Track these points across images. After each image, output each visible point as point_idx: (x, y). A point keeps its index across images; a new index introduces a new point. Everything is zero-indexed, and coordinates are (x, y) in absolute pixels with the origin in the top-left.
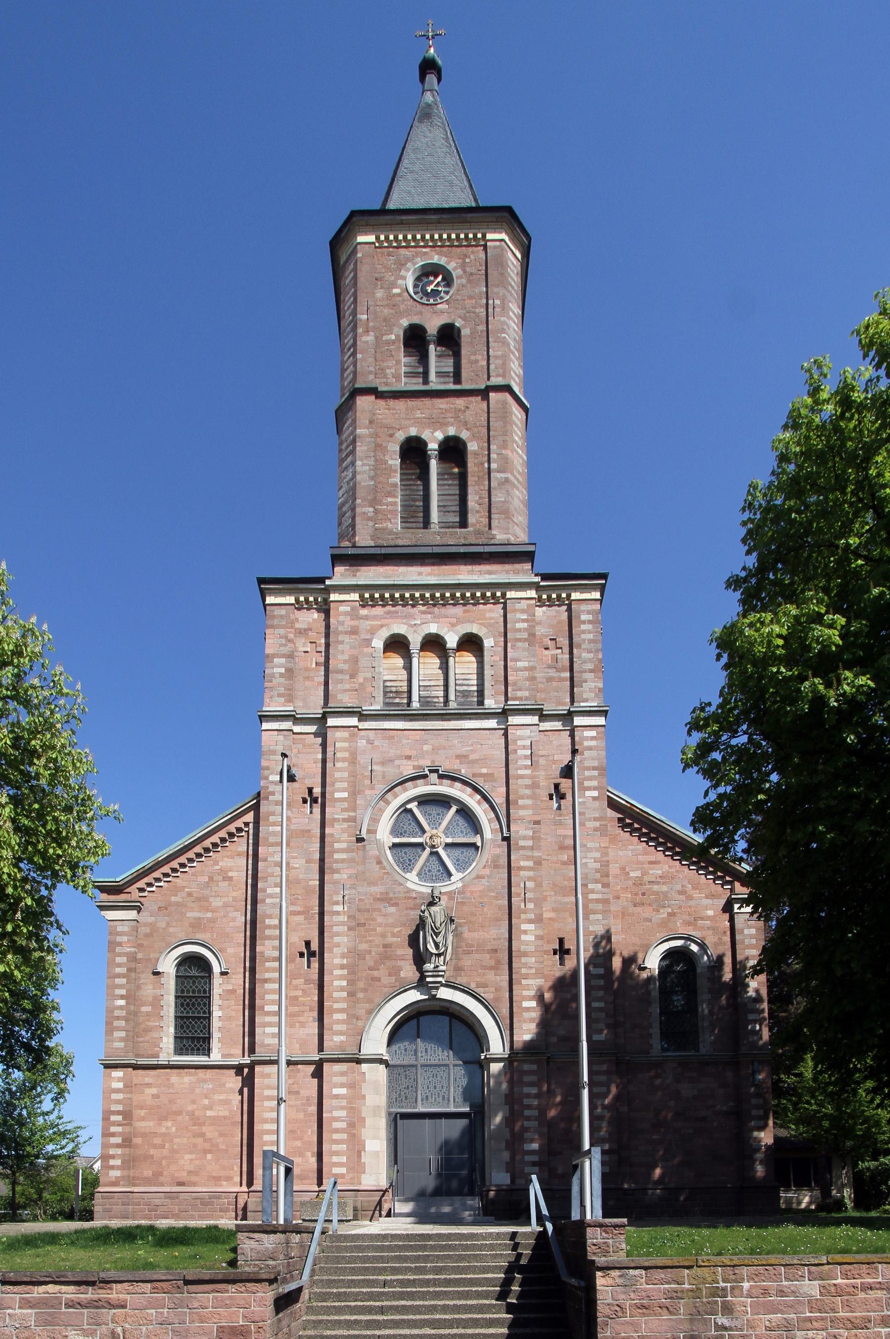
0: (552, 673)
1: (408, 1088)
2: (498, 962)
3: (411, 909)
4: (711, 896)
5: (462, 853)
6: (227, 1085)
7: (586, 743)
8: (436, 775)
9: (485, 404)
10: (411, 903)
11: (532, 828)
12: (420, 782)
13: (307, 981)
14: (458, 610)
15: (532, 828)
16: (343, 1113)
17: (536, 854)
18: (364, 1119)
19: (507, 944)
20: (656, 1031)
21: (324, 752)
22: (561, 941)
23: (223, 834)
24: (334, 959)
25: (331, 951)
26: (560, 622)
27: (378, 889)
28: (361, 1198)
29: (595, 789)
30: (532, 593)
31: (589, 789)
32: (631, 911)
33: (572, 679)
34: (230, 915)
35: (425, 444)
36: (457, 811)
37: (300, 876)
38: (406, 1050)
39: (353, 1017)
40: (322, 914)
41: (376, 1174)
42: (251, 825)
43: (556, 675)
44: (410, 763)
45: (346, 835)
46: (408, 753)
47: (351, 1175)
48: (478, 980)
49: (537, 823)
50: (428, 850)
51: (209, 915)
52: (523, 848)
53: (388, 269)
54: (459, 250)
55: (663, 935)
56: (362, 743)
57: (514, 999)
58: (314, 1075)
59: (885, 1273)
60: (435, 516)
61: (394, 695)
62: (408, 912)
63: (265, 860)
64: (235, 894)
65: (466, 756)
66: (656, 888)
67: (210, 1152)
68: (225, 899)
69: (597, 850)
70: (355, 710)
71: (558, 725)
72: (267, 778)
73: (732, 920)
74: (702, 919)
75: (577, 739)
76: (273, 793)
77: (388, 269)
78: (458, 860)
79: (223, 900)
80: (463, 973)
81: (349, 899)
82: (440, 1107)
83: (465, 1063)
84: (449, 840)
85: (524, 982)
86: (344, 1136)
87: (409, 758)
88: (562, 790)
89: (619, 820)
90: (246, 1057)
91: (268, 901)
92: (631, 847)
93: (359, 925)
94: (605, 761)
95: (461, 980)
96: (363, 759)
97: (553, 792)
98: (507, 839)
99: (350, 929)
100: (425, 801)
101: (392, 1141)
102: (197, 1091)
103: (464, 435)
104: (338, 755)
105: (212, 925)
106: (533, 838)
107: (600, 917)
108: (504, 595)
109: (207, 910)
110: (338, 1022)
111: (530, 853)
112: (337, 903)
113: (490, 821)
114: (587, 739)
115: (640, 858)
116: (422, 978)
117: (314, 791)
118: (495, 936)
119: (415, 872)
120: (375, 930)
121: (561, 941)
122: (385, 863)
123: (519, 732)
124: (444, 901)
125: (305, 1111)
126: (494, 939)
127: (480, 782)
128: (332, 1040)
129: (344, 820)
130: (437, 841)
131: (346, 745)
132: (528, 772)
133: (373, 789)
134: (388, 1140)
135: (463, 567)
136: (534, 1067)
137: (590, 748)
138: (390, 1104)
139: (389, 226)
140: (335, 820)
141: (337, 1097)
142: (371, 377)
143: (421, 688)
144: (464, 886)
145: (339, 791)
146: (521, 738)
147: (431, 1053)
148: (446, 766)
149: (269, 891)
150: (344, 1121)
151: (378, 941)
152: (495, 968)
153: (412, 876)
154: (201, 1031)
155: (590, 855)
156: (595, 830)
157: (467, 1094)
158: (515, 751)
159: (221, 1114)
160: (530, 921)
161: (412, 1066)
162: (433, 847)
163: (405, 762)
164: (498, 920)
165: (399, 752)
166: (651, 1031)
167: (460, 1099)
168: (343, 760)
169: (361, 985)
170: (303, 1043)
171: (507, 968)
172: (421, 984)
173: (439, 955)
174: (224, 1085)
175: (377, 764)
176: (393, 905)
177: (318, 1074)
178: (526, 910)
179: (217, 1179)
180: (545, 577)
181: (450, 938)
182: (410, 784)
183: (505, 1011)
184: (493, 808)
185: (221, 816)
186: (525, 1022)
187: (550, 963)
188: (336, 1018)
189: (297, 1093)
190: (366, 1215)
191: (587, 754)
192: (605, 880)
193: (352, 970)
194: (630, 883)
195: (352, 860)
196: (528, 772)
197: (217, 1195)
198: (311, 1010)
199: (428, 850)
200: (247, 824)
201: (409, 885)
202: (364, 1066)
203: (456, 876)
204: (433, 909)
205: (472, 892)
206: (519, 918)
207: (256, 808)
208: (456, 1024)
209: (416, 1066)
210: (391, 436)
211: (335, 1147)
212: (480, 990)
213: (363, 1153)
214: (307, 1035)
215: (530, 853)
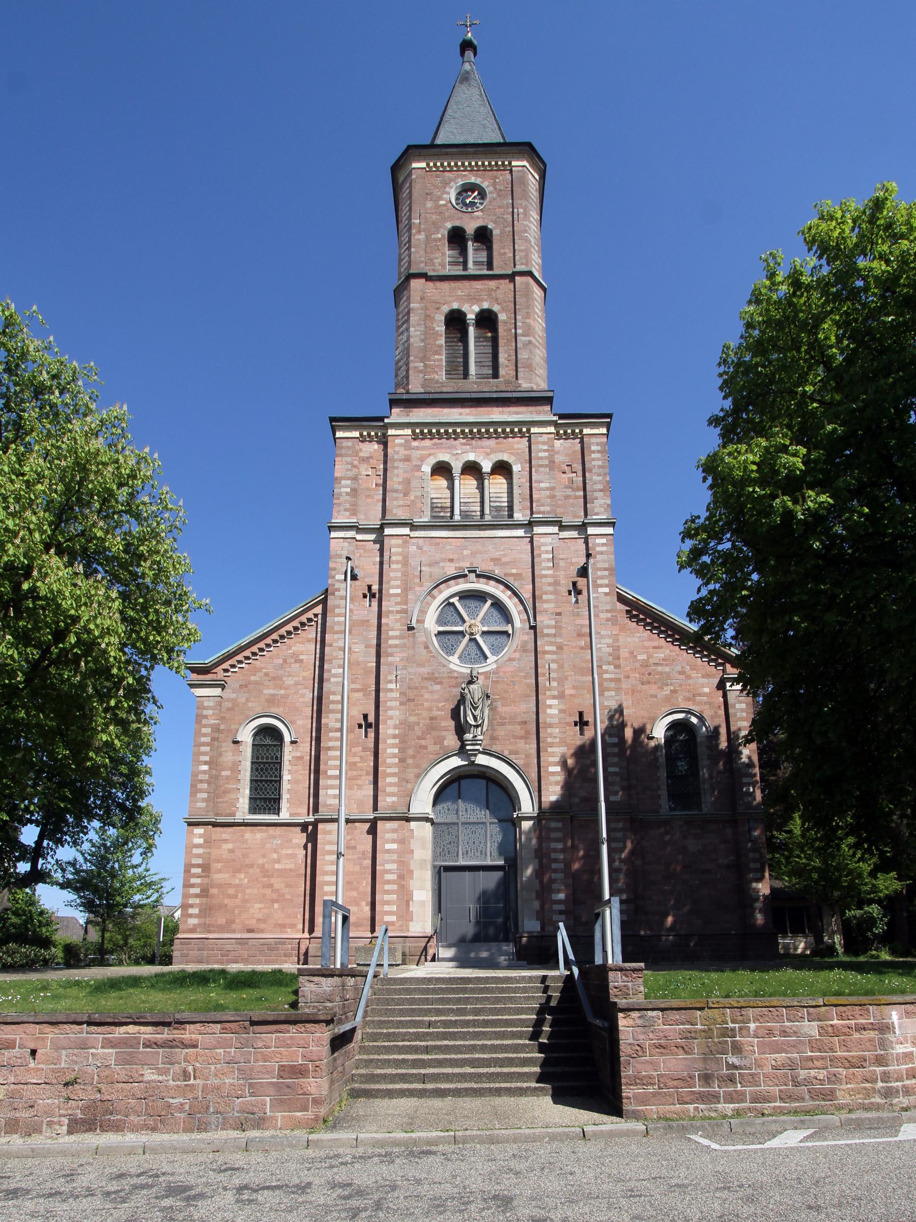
4: (707, 676)
6: (294, 841)
7: (598, 549)
9: (512, 285)
10: (454, 682)
13: (365, 749)
14: (492, 442)
16: (394, 866)
17: (559, 640)
18: (412, 872)
19: (535, 717)
20: (664, 792)
21: (382, 556)
22: (581, 714)
23: (296, 623)
24: (388, 729)
26: (574, 452)
27: (425, 670)
28: (409, 943)
29: (606, 586)
30: (552, 429)
31: (601, 586)
33: (585, 497)
34: (300, 692)
35: (465, 315)
36: (492, 604)
38: (449, 810)
39: (403, 780)
40: (378, 691)
41: (423, 922)
42: (320, 616)
45: (399, 624)
47: (400, 923)
49: (559, 614)
51: (282, 692)
52: (548, 635)
53: (436, 187)
56: (413, 549)
58: (369, 832)
62: (451, 689)
63: (331, 645)
64: (304, 674)
65: (499, 559)
66: (660, 669)
69: (609, 637)
71: (574, 534)
72: (334, 577)
73: (725, 696)
74: (700, 695)
75: (590, 545)
77: (436, 187)
78: (493, 645)
83: (500, 821)
84: (485, 629)
85: (550, 750)
86: (395, 887)
87: (451, 560)
89: (627, 612)
91: (332, 680)
92: (637, 635)
93: (409, 700)
95: (496, 748)
96: (414, 562)
98: (533, 628)
99: (401, 704)
100: (465, 596)
101: (437, 892)
102: (268, 846)
103: (496, 308)
104: (393, 558)
105: (284, 700)
106: (555, 627)
107: (613, 693)
108: (528, 431)
109: (281, 688)
110: (391, 785)
111: (553, 640)
112: (391, 682)
113: (519, 613)
114: (599, 545)
115: (646, 643)
116: (463, 746)
119: (456, 656)
121: (581, 714)
122: (431, 648)
123: (543, 540)
125: (361, 864)
126: (524, 713)
127: (511, 581)
129: (398, 612)
130: (475, 630)
131: (400, 550)
133: (422, 586)
134: (433, 890)
135: (495, 409)
136: (560, 825)
137: (601, 553)
138: (435, 857)
139: (437, 156)
140: (390, 612)
141: (389, 851)
142: (422, 265)
144: (498, 668)
145: (393, 587)
146: (544, 545)
147: (470, 812)
148: (482, 567)
149: (333, 671)
151: (425, 714)
152: (525, 737)
153: (454, 659)
155: (603, 641)
156: (608, 620)
158: (540, 555)
159: (288, 867)
160: (554, 697)
161: (454, 824)
162: (472, 634)
163: (448, 564)
164: (527, 696)
165: (443, 556)
166: (660, 792)
168: (398, 562)
169: (410, 752)
170: (360, 804)
171: (535, 736)
172: (462, 751)
174: (291, 841)
175: (425, 566)
176: (437, 684)
177: (373, 831)
178: (550, 687)
179: (283, 927)
180: (561, 417)
182: (452, 582)
183: (534, 775)
187: (572, 733)
188: (388, 782)
189: (354, 848)
191: (599, 557)
192: (617, 662)
193: (403, 739)
194: (638, 665)
195: (403, 646)
196: (550, 572)
200: (316, 615)
201: (452, 666)
203: (492, 659)
204: (472, 687)
205: (505, 672)
206: (545, 694)
207: (324, 602)
209: (457, 824)
213: (411, 902)
214: (364, 796)
215: (553, 640)
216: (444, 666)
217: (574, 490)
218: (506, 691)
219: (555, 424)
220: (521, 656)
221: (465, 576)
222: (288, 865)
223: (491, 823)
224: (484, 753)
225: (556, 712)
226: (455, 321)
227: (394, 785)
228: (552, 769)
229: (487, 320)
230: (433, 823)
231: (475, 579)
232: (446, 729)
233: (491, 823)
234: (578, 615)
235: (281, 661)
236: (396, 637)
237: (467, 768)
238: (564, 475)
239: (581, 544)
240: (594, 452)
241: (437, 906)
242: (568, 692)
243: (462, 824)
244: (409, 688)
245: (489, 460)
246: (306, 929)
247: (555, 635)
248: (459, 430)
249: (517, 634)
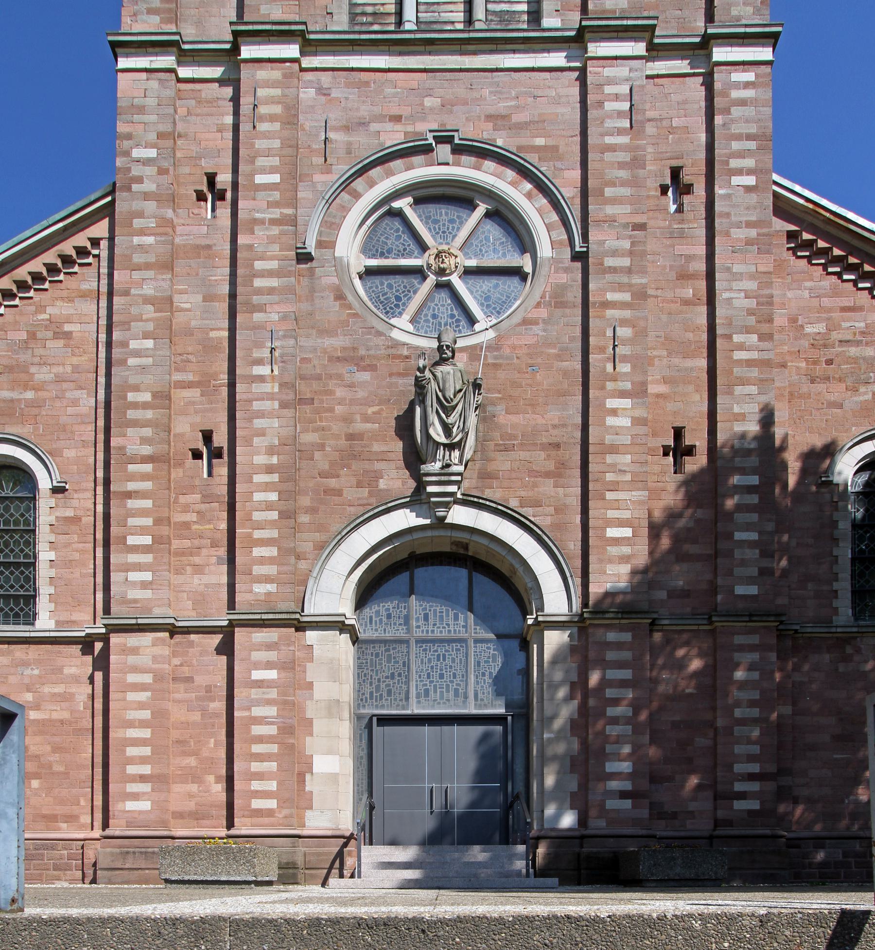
1: (392, 676)
2: (562, 465)
3: (400, 375)
5: (496, 286)
6: (66, 671)
7: (735, 94)
8: (447, 148)
10: (401, 366)
11: (630, 237)
12: (417, 159)
13: (207, 498)
15: (630, 237)
16: (271, 711)
17: (637, 280)
18: (310, 722)
19: (578, 434)
20: (844, 585)
21: (236, 113)
22: (678, 433)
23: (51, 257)
24: (254, 456)
25: (249, 443)
27: (337, 343)
28: (302, 847)
29: (750, 172)
31: (739, 172)
32: (805, 389)
34: (68, 395)
36: (488, 215)
37: (193, 323)
38: (389, 616)
39: (289, 553)
40: (232, 385)
41: (333, 807)
42: (104, 244)
44: (398, 127)
45: (276, 247)
46: (395, 111)
47: (285, 812)
48: (523, 494)
49: (642, 227)
50: (432, 279)
51: (30, 395)
52: (614, 270)
55: (858, 431)
56: (308, 94)
57: (592, 523)
58: (219, 651)
59: (822, 948)
61: (370, 19)
62: (394, 380)
63: (126, 293)
64: (75, 360)
65: (503, 117)
66: (853, 351)
67: (37, 776)
68: (60, 369)
69: (752, 277)
70: (293, 28)
71: (681, 66)
72: (127, 154)
75: (717, 86)
76: (139, 180)
78: (487, 298)
79: (55, 369)
80: (495, 483)
81: (282, 356)
82: (451, 707)
83: (499, 636)
84: (472, 263)
86: (274, 748)
87: (397, 119)
89: (791, 236)
90: (100, 622)
91: (131, 361)
92: (808, 284)
93: (302, 401)
94: (770, 125)
95: (493, 493)
96: (309, 122)
97: (668, 181)
98: (581, 257)
99: (284, 405)
100: (429, 195)
101: (365, 761)
102: (12, 679)
104: (263, 110)
105: (35, 411)
106: (631, 253)
107: (753, 389)
109: (26, 387)
111: (625, 279)
112: (259, 362)
113: (549, 228)
114: (737, 85)
115: (826, 302)
116: (421, 487)
117: (219, 179)
118: (556, 422)
119: (406, 317)
120: (331, 410)
121: (678, 433)
122: (350, 298)
123: (609, 71)
124: (461, 360)
125: (204, 711)
126: (555, 427)
128: (251, 591)
129: (273, 222)
130: (449, 263)
131: (277, 92)
133: (329, 172)
134: (357, 759)
136: (627, 637)
138: (360, 698)
140: (255, 221)
141: (260, 684)
143: (421, 8)
144: (499, 338)
145: (263, 171)
146: (611, 81)
147: (433, 617)
148: (469, 131)
149: (134, 345)
150: (272, 723)
151: (337, 427)
152: (557, 474)
153: (403, 321)
154: (22, 587)
155: (735, 285)
156: (749, 242)
157: (500, 685)
158: (600, 104)
159: (55, 716)
160: (623, 394)
161: (400, 641)
162: (441, 272)
163: (389, 126)
165: (377, 110)
166: (836, 586)
167: (487, 689)
168: (272, 118)
169: (305, 501)
170: (200, 600)
171: (577, 472)
172: (418, 499)
174: (60, 670)
175: (336, 129)
176: (364, 369)
177: (227, 648)
178: (614, 374)
179: (51, 819)
181: (472, 420)
182: (398, 163)
183: (574, 546)
184: (556, 205)
185: (45, 223)
186: (610, 561)
187: (657, 469)
188: (260, 553)
189: (190, 680)
190: (313, 877)
191: (736, 112)
192: (765, 328)
193: (289, 480)
194: (806, 344)
195: (289, 290)
196: (624, 140)
198: (214, 545)
199: (432, 279)
200: (95, 242)
201: (396, 334)
202: (311, 636)
204: (441, 370)
205: (514, 347)
206: (603, 388)
207: (109, 211)
208: (482, 582)
209: (407, 642)
211: (255, 767)
212: (528, 511)
213: (308, 777)
214: (206, 586)
215: (625, 279)
216: (379, 334)
218: (515, 384)
220: (551, 316)
221: (427, 150)
223: (477, 641)
224: (465, 502)
225: (625, 422)
227: (271, 561)
230: (355, 640)
231: (450, 158)
232: (383, 457)
233: (477, 641)
234: (682, 235)
235: (24, 336)
236: (270, 274)
237: (429, 533)
239: (695, 89)
241: (365, 782)
242: (653, 389)
243: (420, 641)
244: (303, 378)
246: (98, 823)
249: (543, 271)
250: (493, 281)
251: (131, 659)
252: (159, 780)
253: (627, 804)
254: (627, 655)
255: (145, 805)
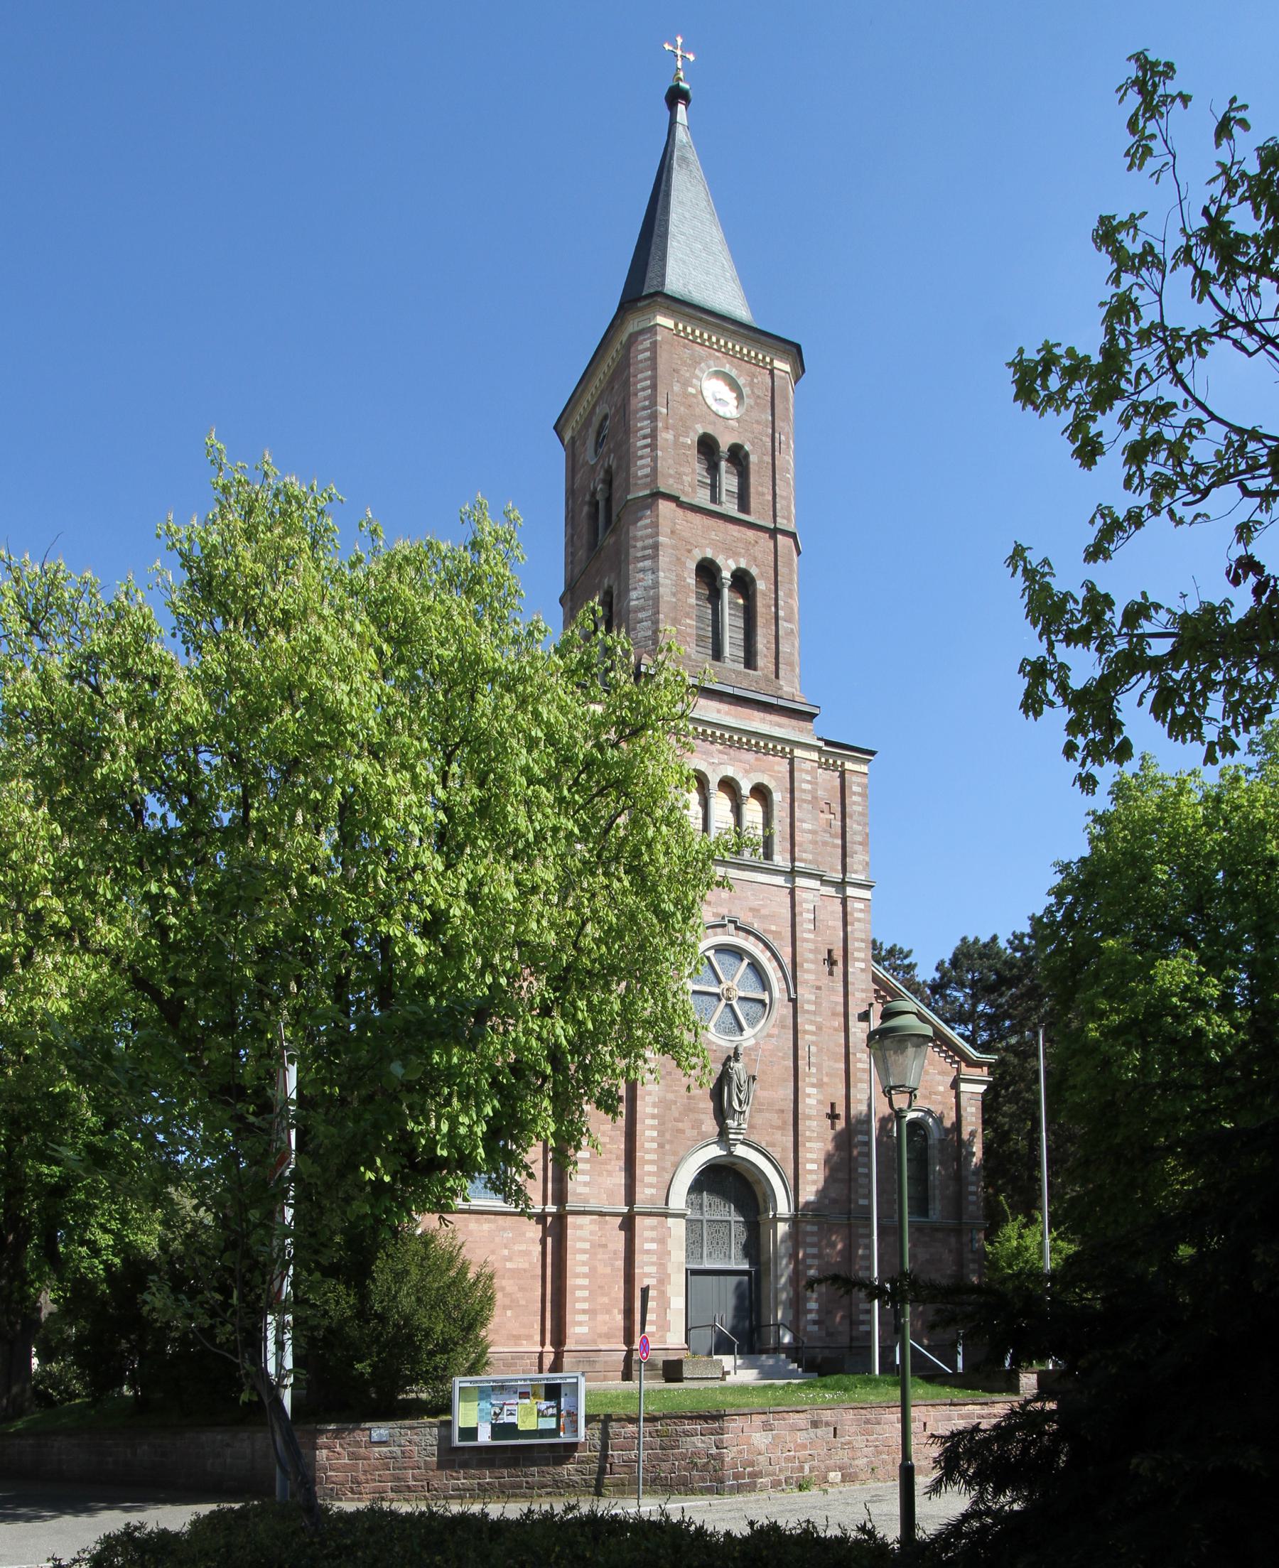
0: (827, 838)
2: (785, 1123)
4: (942, 1073)
9: (771, 544)
12: (719, 930)
14: (750, 757)
17: (819, 1019)
22: (833, 1105)
25: (643, 1099)
26: (833, 787)
30: (815, 756)
33: (844, 847)
35: (719, 570)
43: (830, 840)
49: (819, 988)
50: (724, 1002)
52: (808, 1012)
53: (684, 363)
54: (748, 366)
58: (621, 1228)
60: (727, 650)
65: (758, 911)
67: (510, 1308)
73: (958, 1096)
74: (935, 1094)
77: (684, 363)
84: (742, 994)
85: (808, 1145)
88: (835, 957)
89: (876, 991)
95: (753, 1138)
98: (794, 1001)
100: (721, 949)
103: (754, 571)
108: (791, 752)
110: (649, 1174)
125: (612, 1265)
127: (769, 938)
132: (811, 936)
135: (756, 713)
136: (815, 1228)
137: (859, 920)
139: (689, 318)
141: (648, 1252)
142: (671, 481)
144: (757, 1043)
146: (806, 901)
148: (744, 918)
158: (801, 914)
159: (521, 1266)
160: (813, 1085)
162: (729, 999)
164: (785, 1080)
169: (668, 1136)
171: (791, 1128)
173: (741, 1113)
174: (524, 1234)
179: (517, 1338)
180: (828, 743)
189: (605, 1246)
191: (857, 925)
197: (519, 1356)
198: (617, 1158)
203: (748, 1032)
210: (689, 551)
217: (832, 836)
219: (819, 750)
221: (724, 926)
222: (521, 1263)
225: (814, 1102)
226: (707, 571)
228: (810, 1166)
229: (743, 582)
232: (704, 1112)
238: (822, 815)
240: (855, 794)
245: (749, 779)
247: (815, 1013)
248: (718, 734)
249: (776, 1005)
250: (751, 1004)
251: (579, 1233)
252: (591, 1312)
253: (816, 1328)
254: (815, 1239)
255: (585, 1330)
